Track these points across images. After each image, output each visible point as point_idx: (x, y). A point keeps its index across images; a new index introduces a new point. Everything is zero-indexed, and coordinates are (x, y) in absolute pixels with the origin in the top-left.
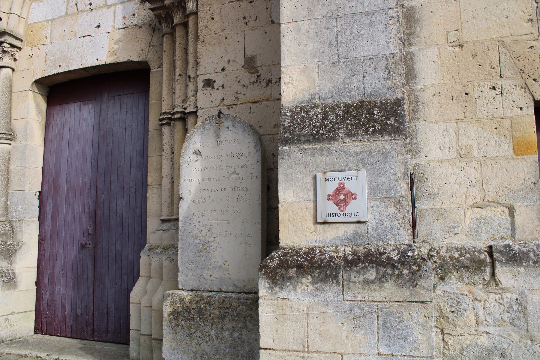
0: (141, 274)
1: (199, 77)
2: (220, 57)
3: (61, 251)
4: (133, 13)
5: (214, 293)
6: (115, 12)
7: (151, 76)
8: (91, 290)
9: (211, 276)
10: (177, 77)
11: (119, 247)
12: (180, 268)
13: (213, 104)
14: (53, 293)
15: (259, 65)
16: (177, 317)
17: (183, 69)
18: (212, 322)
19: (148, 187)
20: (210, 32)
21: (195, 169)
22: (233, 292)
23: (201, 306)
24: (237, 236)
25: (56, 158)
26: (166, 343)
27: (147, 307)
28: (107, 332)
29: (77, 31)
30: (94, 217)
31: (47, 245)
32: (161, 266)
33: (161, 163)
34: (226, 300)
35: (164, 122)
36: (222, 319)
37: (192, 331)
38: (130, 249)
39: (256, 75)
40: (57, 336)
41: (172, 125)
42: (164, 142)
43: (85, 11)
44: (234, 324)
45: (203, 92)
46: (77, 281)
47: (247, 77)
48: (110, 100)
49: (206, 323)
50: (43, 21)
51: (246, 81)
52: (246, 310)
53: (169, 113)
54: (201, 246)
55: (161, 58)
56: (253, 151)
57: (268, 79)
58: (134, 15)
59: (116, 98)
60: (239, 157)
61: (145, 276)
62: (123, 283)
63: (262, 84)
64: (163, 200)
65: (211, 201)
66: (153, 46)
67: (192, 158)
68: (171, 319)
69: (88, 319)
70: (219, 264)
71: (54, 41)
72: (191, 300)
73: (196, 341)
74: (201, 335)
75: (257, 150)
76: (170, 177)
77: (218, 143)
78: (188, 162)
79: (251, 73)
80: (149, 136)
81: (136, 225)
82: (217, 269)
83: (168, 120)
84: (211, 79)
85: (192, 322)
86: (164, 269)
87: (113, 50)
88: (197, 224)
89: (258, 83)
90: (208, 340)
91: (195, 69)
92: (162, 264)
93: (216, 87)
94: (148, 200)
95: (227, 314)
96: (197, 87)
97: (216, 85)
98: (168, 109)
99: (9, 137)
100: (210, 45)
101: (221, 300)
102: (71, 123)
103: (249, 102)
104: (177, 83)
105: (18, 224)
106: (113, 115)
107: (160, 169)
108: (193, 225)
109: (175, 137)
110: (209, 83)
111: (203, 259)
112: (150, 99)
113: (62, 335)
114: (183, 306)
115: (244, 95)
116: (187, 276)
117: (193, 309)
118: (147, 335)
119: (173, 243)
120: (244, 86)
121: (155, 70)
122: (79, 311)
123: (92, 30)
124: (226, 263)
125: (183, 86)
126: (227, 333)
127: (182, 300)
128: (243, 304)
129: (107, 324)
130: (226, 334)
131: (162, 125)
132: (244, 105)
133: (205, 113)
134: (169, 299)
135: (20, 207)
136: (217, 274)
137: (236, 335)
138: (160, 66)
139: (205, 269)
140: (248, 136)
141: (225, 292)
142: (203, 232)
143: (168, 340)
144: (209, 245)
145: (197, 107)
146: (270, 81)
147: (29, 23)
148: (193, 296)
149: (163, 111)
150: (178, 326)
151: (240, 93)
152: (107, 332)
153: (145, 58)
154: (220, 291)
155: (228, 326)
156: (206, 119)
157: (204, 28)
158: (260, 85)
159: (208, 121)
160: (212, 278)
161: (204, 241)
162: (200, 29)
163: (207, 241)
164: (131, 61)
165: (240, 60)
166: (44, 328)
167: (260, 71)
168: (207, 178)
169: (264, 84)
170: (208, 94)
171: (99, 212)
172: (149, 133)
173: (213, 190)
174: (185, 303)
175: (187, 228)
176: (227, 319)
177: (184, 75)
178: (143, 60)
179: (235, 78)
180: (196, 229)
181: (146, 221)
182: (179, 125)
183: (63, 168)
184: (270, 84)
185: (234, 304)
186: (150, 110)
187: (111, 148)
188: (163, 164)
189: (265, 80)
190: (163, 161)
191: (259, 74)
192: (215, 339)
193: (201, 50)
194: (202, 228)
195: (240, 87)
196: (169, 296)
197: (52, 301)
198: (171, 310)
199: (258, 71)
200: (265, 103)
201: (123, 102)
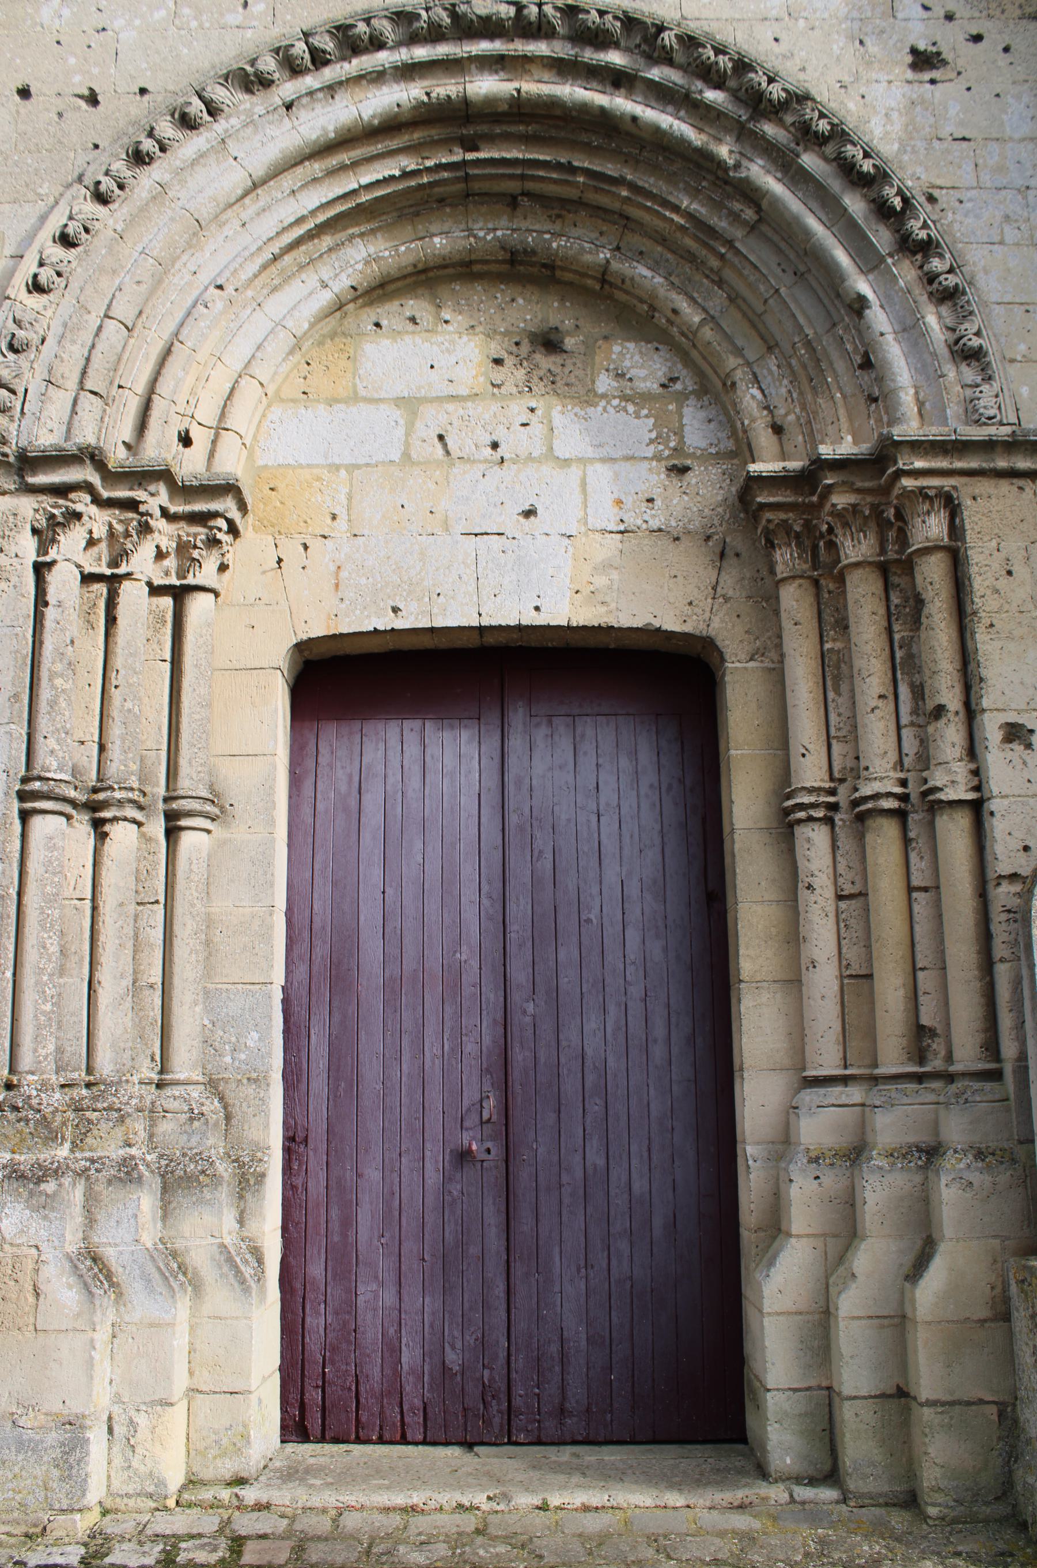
3: (373, 1174)
4: (647, 496)
6: (584, 484)
8: (500, 1290)
11: (596, 1158)
14: (350, 1306)
20: (1006, 607)
25: (334, 884)
27: (859, 1318)
28: (562, 1412)
29: (450, 514)
30: (501, 1068)
31: (315, 1158)
38: (634, 1162)
40: (368, 1441)
43: (474, 461)
45: (1002, 755)
46: (448, 1266)
48: (538, 725)
50: (317, 466)
58: (650, 500)
59: (556, 721)
61: (808, 1236)
62: (614, 1262)
66: (727, 599)
69: (492, 1379)
71: (366, 532)
80: (737, 846)
84: (1022, 726)
87: (592, 588)
99: (208, 808)
100: (1010, 637)
102: (391, 780)
105: (250, 1090)
106: (551, 769)
112: (732, 744)
113: (387, 1436)
118: (865, 1398)
121: (738, 665)
122: (453, 1358)
123: (510, 521)
129: (563, 1389)
133: (1014, 807)
135: (255, 1035)
147: (260, 463)
152: (562, 1412)
157: (988, 592)
162: (978, 594)
164: (658, 630)
166: (314, 1422)
170: (1017, 761)
171: (519, 1056)
172: (736, 836)
178: (697, 633)
183: (370, 915)
187: (549, 866)
197: (349, 1332)
201: (583, 736)
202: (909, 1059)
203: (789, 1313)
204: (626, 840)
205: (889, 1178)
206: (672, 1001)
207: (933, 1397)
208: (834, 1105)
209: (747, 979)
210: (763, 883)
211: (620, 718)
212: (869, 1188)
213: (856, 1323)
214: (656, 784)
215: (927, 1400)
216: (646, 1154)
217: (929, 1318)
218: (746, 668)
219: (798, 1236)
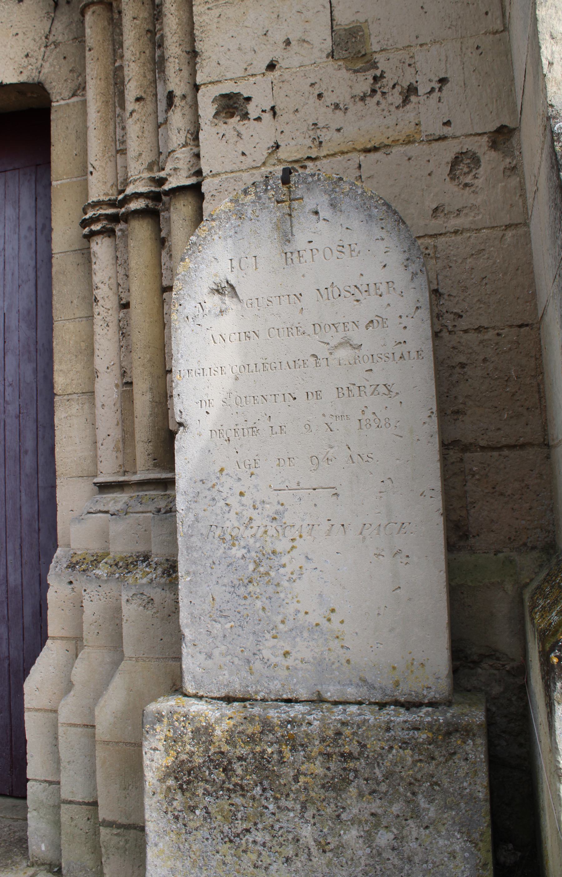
0: (50, 633)
1: (202, 90)
2: (261, 32)
5: (299, 707)
7: (53, 117)
9: (286, 654)
10: (130, 105)
12: (186, 632)
13: (248, 162)
15: (376, 47)
16: (189, 782)
17: (146, 83)
18: (302, 798)
19: (57, 399)
21: (218, 338)
22: (360, 703)
23: (264, 751)
24: (366, 532)
26: (158, 862)
27: (75, 725)
32: (115, 615)
33: (91, 335)
34: (347, 731)
35: (96, 227)
36: (334, 788)
37: (240, 826)
38: (10, 558)
39: (370, 74)
41: (119, 234)
42: (96, 279)
44: (376, 806)
45: (214, 130)
47: (343, 83)
49: (283, 803)
51: (342, 94)
52: (415, 762)
53: (112, 204)
54: (251, 567)
55: (79, 71)
56: (400, 276)
57: (405, 85)
60: (358, 296)
61: (62, 638)
63: (390, 99)
64: (101, 434)
65: (277, 429)
66: (56, 44)
67: (207, 306)
68: (169, 788)
70: (313, 619)
72: (231, 732)
73: (254, 857)
74: (268, 838)
75: (414, 275)
76: (116, 371)
77: (288, 257)
78: (195, 317)
79: (356, 71)
80: (54, 270)
81: (23, 497)
82: (306, 634)
83: (109, 220)
84: (238, 94)
85: (238, 800)
86: (125, 626)
88: (234, 501)
89: (378, 96)
90: (291, 853)
91: (185, 73)
92: (119, 609)
93: (253, 114)
94: (57, 433)
95: (352, 775)
96: (197, 116)
97: (253, 110)
98: (106, 194)
101: (331, 733)
103: (355, 149)
104: (130, 121)
107: (90, 352)
108: (222, 503)
109: (133, 264)
110: (232, 106)
111: (259, 604)
112: (53, 176)
114: (207, 750)
115: (338, 130)
116: (209, 656)
117: (240, 759)
118: (79, 803)
119: (141, 548)
120: (337, 106)
121: (62, 102)
124: (333, 616)
125: (150, 127)
126: (354, 832)
127: (203, 733)
128: (405, 744)
130: (351, 835)
131: (93, 234)
132: (339, 158)
133: (225, 185)
134: (162, 731)
136: (304, 649)
137: (384, 838)
138: (80, 89)
139: (268, 636)
140: (383, 234)
141: (336, 703)
142: (254, 524)
143: (163, 852)
144: (276, 562)
145: (199, 173)
146: (412, 90)
148: (238, 718)
149: (93, 198)
150: (192, 809)
151: (327, 127)
153: (35, 74)
154: (318, 700)
155: (355, 811)
156: (246, 192)
158: (383, 102)
159: (251, 197)
160: (290, 661)
161: (261, 551)
163: (268, 549)
165: (322, 38)
167: (382, 65)
168: (260, 362)
169: (396, 98)
170: (231, 135)
172: (54, 261)
173: (280, 398)
174: (211, 742)
175: (202, 514)
176: (353, 790)
177: (149, 99)
178: (31, 81)
179: (307, 88)
180: (232, 515)
181: (54, 487)
182: (140, 231)
184: (413, 98)
185: (374, 745)
186: (53, 202)
188: (97, 337)
189: (398, 88)
190: (98, 329)
191: (378, 73)
192: (314, 851)
193: (205, 17)
194: (249, 513)
195: (324, 109)
196: (160, 721)
198: (169, 761)
199: (374, 65)
200: (402, 149)
202: (155, 465)
203: (46, 711)
204: (9, 277)
205: (106, 588)
206: (40, 416)
207: (110, 818)
208: (100, 512)
209: (60, 392)
210: (75, 302)
211: (8, 173)
212: (87, 597)
213: (73, 730)
214: (33, 227)
215: (104, 820)
216: (18, 552)
217: (107, 738)
218: (68, 105)
219: (54, 638)
